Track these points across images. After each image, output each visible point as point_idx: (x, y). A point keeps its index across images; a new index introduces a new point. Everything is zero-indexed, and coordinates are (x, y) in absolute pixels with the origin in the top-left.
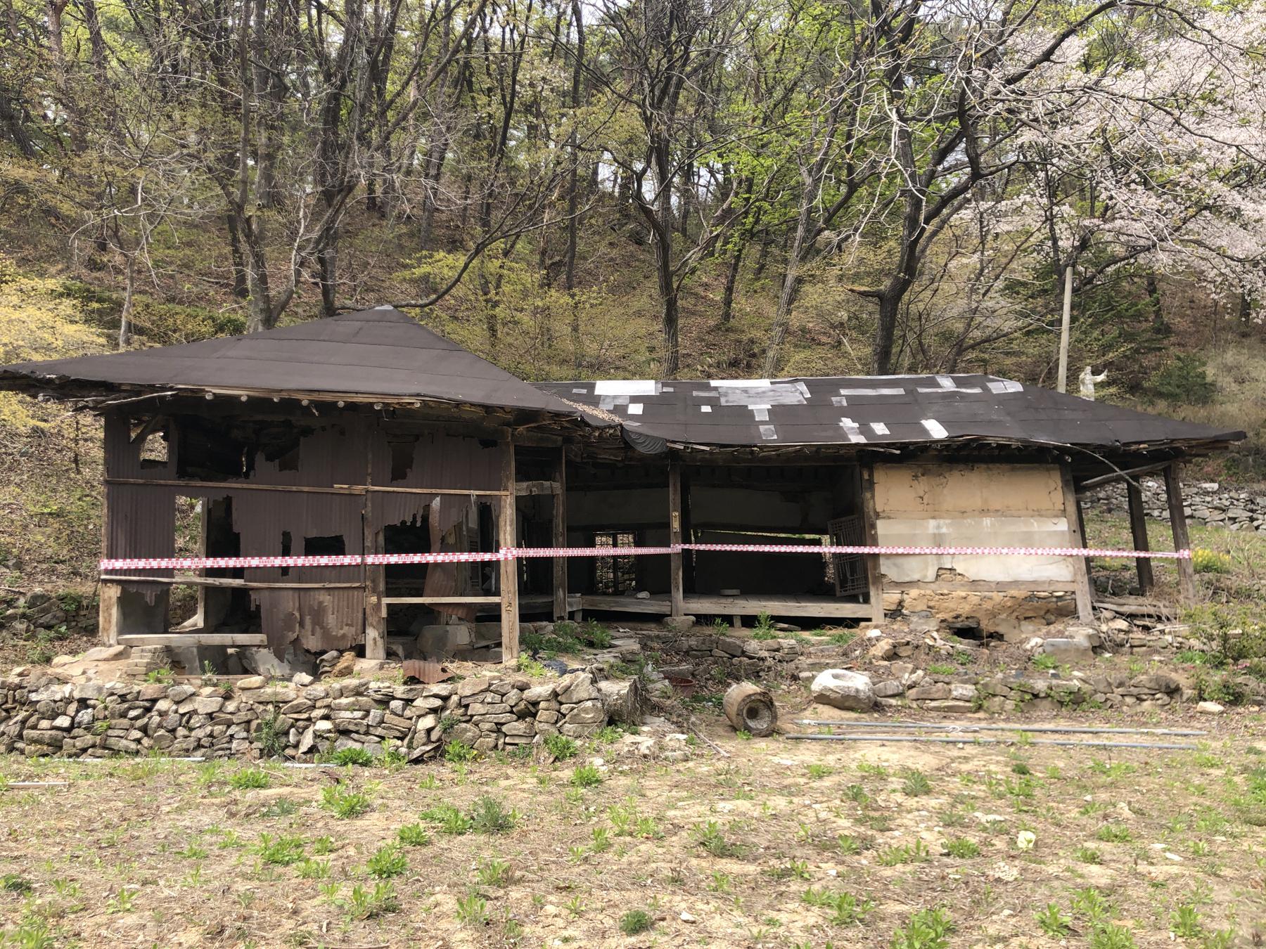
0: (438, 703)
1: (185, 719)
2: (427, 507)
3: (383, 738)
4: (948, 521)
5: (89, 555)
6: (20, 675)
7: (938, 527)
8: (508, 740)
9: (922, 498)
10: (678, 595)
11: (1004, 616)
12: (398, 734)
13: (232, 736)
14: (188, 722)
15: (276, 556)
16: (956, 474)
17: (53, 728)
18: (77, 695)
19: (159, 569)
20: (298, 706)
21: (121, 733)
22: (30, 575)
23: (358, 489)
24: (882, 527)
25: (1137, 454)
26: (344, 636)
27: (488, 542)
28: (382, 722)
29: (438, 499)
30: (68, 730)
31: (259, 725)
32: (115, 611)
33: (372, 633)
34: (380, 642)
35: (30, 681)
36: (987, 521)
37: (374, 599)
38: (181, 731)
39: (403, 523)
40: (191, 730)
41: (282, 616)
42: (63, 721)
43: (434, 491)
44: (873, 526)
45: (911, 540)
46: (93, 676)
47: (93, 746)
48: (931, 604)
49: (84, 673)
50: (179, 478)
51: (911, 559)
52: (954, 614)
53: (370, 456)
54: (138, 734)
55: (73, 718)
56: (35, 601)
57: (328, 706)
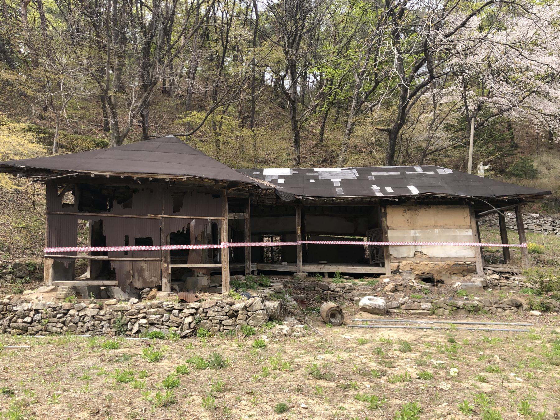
0: (194, 311)
1: (82, 318)
2: (189, 224)
3: (169, 327)
4: (419, 231)
5: (39, 246)
6: (9, 299)
7: (415, 233)
8: (225, 327)
9: (408, 220)
10: (300, 263)
11: (444, 273)
12: (176, 325)
13: (102, 326)
14: (83, 319)
15: (122, 246)
16: (423, 210)
17: (24, 322)
18: (34, 308)
19: (70, 252)
20: (132, 312)
21: (54, 324)
22: (13, 254)
23: (159, 216)
24: (390, 233)
25: (503, 201)
26: (152, 281)
27: (216, 240)
28: (169, 319)
29: (194, 221)
30: (30, 323)
31: (114, 321)
32: (51, 271)
33: (165, 280)
34: (168, 284)
35: (13, 301)
36: (437, 231)
37: (165, 265)
38: (80, 324)
39: (178, 231)
40: (84, 323)
41: (125, 273)
42: (28, 319)
43: (192, 217)
44: (386, 233)
45: (403, 239)
46: (41, 299)
47: (41, 330)
48: (412, 267)
49: (37, 298)
50: (79, 212)
51: (403, 247)
52: (422, 272)
53: (164, 202)
54: (61, 325)
55: (32, 318)
56: (15, 266)
57: (145, 313)
